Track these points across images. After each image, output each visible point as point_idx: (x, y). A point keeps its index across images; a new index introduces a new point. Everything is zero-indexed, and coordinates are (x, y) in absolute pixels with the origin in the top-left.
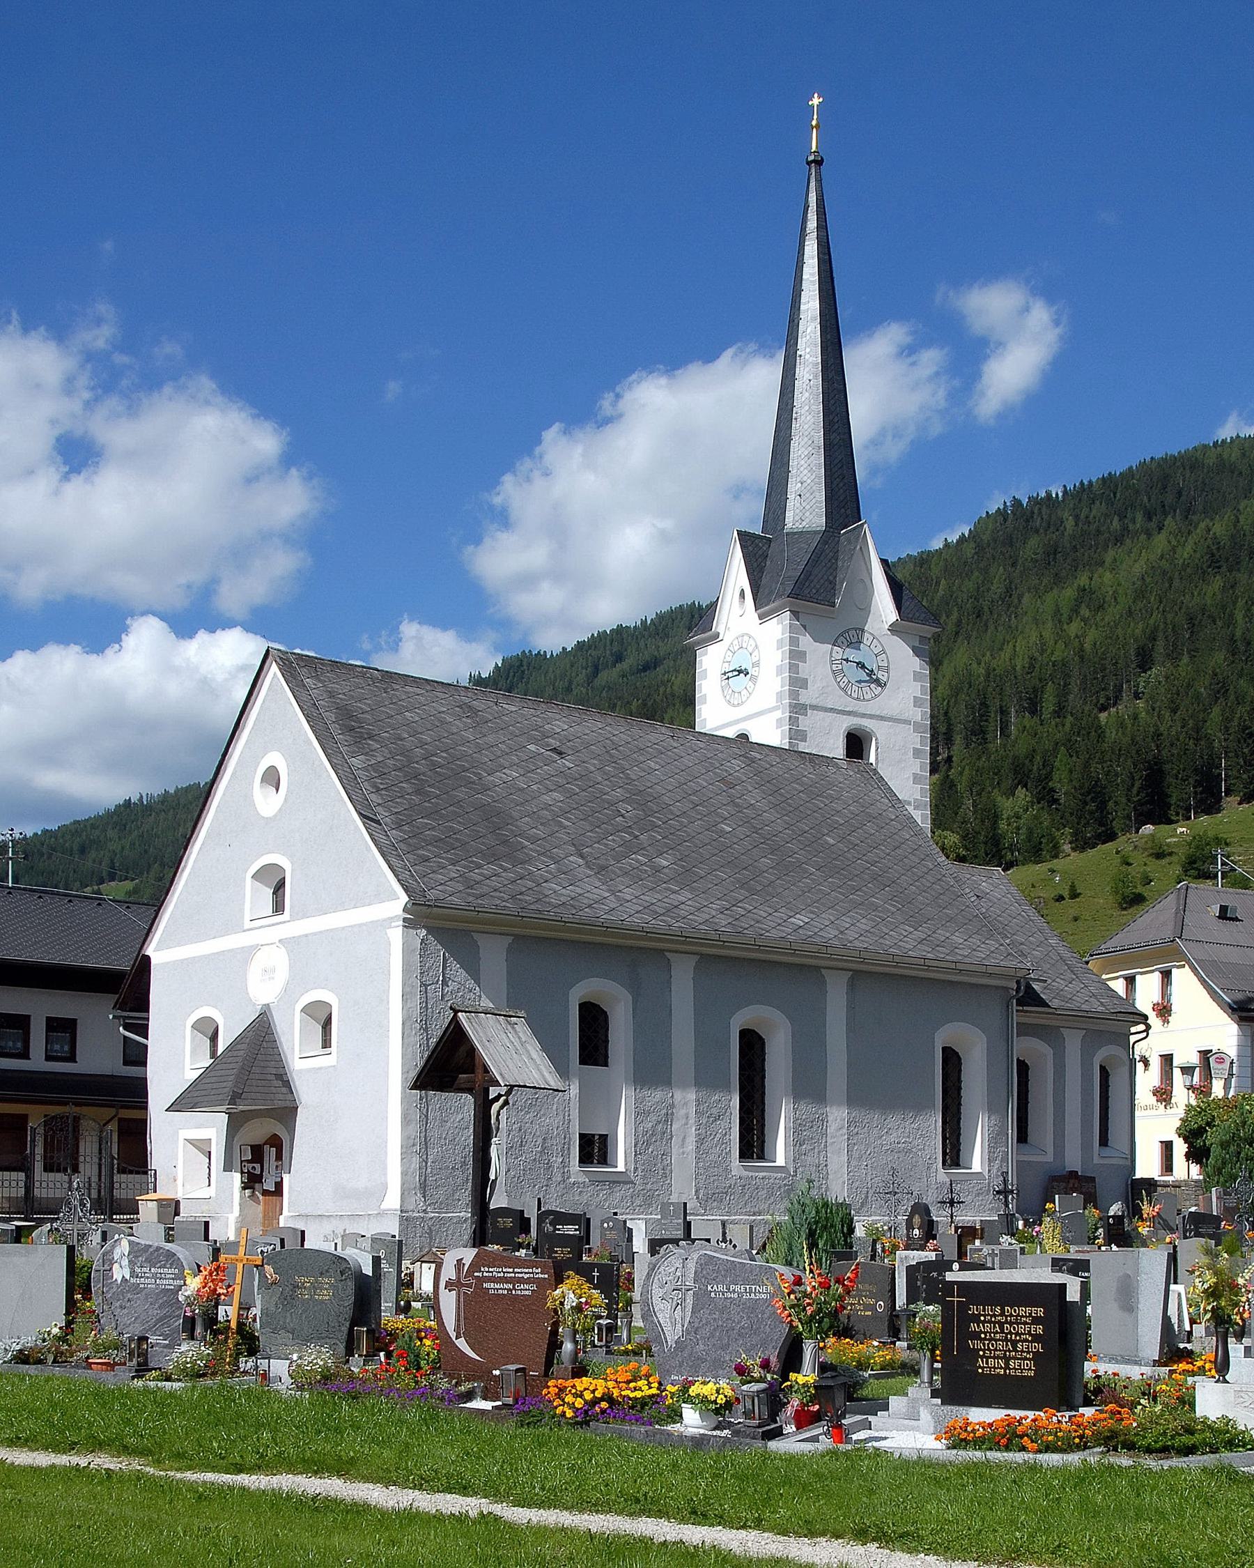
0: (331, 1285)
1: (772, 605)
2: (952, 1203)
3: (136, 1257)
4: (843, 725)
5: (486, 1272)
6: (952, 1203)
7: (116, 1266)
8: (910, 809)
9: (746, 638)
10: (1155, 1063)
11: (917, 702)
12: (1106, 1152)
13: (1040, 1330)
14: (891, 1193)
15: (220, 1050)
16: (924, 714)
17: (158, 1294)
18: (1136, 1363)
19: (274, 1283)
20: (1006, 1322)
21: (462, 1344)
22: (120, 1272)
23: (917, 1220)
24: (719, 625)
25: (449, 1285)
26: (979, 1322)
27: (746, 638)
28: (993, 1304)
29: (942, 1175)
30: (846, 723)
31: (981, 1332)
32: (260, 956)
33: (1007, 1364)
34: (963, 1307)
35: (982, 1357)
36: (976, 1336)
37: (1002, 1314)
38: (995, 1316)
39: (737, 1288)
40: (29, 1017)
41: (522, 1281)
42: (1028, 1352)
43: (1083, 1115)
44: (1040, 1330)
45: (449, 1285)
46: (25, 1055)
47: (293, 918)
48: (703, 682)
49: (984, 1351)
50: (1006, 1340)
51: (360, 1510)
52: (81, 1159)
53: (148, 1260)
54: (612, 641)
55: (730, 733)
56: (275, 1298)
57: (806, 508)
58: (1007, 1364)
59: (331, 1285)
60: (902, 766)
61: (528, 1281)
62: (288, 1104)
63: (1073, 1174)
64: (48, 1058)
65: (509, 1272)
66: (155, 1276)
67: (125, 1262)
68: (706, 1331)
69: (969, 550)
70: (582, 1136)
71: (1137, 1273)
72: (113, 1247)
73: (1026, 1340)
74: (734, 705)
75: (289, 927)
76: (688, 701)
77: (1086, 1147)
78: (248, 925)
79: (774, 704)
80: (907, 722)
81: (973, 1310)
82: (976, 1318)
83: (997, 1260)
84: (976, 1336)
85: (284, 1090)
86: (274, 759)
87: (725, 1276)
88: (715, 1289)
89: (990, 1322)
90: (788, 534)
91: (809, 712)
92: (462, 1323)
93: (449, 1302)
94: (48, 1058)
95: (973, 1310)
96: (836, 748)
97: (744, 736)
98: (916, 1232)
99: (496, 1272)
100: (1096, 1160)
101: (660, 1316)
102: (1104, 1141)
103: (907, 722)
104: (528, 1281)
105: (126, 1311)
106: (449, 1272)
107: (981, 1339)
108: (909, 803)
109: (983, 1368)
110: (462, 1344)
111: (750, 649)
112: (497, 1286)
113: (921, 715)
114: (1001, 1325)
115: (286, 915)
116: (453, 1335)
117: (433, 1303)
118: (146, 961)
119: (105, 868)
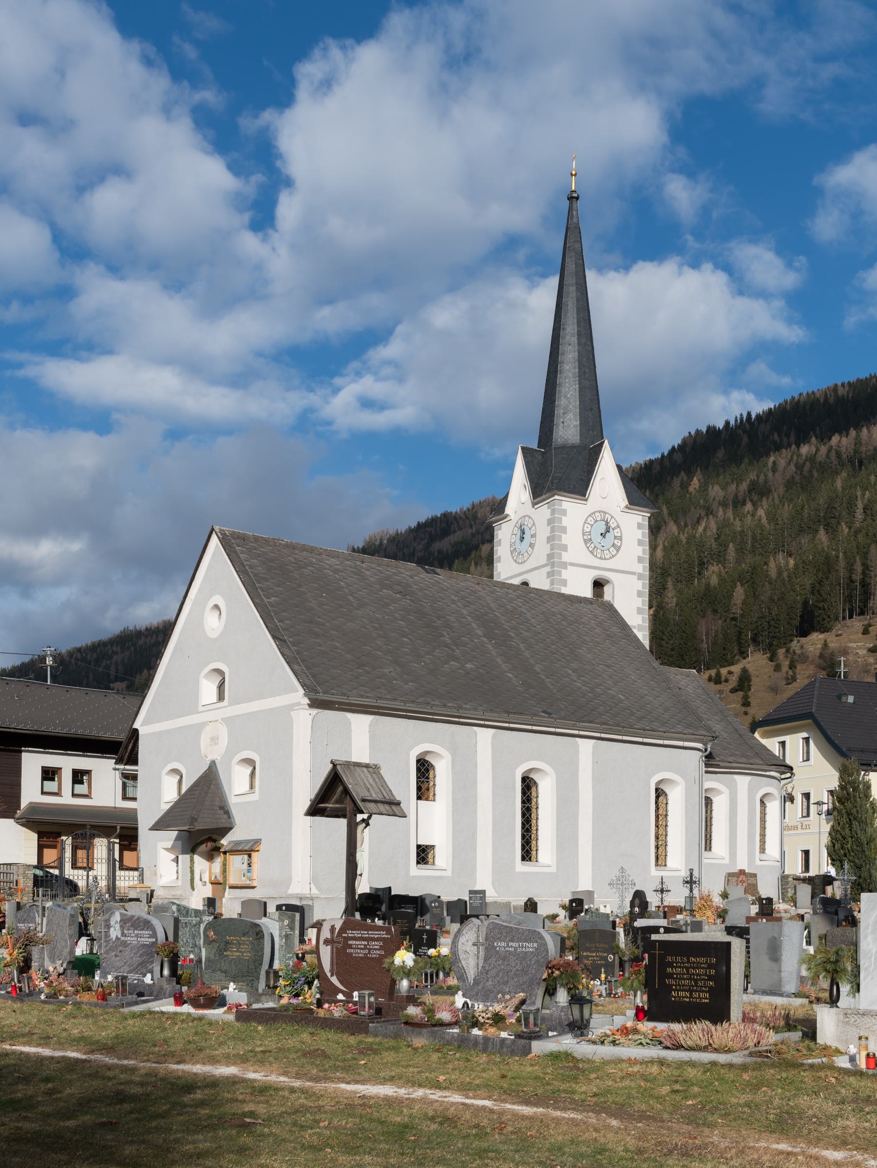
0: (251, 942)
1: (544, 496)
2: (662, 891)
3: (125, 923)
4: (591, 576)
5: (350, 933)
6: (662, 891)
7: (112, 929)
8: (635, 631)
9: (527, 518)
10: (799, 798)
11: (640, 560)
12: (763, 857)
13: (669, 970)
14: (619, 882)
15: (183, 791)
16: (644, 567)
17: (139, 948)
18: (781, 995)
19: (214, 941)
20: (691, 967)
21: (334, 980)
22: (115, 933)
23: (637, 901)
24: (509, 509)
25: (327, 942)
26: (672, 967)
27: (527, 518)
28: (682, 955)
29: (655, 873)
30: (593, 574)
31: (674, 974)
32: (209, 728)
33: (691, 994)
34: (662, 958)
35: (675, 990)
36: (670, 976)
37: (688, 962)
38: (683, 963)
39: (513, 944)
40: (43, 767)
41: (373, 939)
42: (705, 987)
43: (749, 833)
44: (669, 970)
45: (327, 942)
46: (57, 794)
47: (231, 704)
48: (499, 548)
49: (676, 986)
50: (690, 979)
51: (527, 1102)
52: (95, 861)
53: (132, 926)
54: (441, 521)
55: (516, 581)
56: (214, 950)
57: (568, 429)
58: (691, 994)
59: (251, 942)
60: (631, 603)
61: (377, 940)
62: (228, 826)
63: (742, 872)
64: (74, 795)
65: (365, 934)
66: (137, 936)
67: (118, 926)
68: (493, 973)
69: (678, 457)
70: (418, 847)
71: (780, 935)
72: (110, 917)
73: (704, 979)
74: (519, 563)
75: (228, 710)
76: (490, 560)
77: (751, 854)
78: (201, 709)
79: (545, 562)
80: (633, 573)
81: (669, 959)
82: (670, 965)
83: (689, 928)
84: (670, 976)
85: (225, 816)
86: (218, 600)
87: (506, 937)
88: (500, 945)
89: (680, 967)
90: (555, 448)
91: (569, 567)
92: (335, 967)
93: (326, 953)
94: (74, 795)
95: (669, 959)
96: (587, 592)
97: (525, 584)
98: (637, 909)
99: (357, 934)
100: (758, 862)
101: (463, 962)
102: (763, 850)
103: (633, 573)
104: (377, 940)
105: (118, 958)
106: (326, 934)
107: (674, 978)
108: (635, 627)
109: (675, 997)
110: (334, 980)
111: (530, 526)
112: (358, 943)
113: (643, 568)
114: (687, 969)
115: (225, 702)
116: (329, 974)
117: (316, 951)
118: (136, 731)
119: (112, 672)
